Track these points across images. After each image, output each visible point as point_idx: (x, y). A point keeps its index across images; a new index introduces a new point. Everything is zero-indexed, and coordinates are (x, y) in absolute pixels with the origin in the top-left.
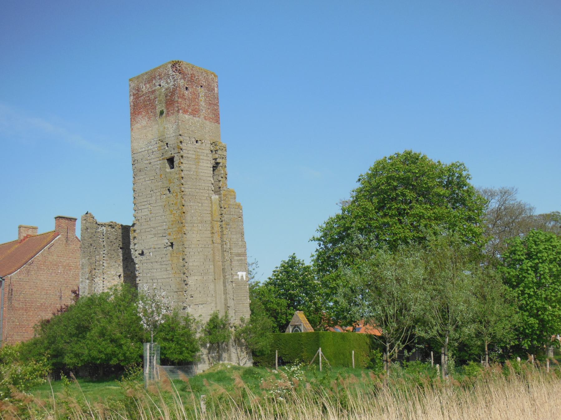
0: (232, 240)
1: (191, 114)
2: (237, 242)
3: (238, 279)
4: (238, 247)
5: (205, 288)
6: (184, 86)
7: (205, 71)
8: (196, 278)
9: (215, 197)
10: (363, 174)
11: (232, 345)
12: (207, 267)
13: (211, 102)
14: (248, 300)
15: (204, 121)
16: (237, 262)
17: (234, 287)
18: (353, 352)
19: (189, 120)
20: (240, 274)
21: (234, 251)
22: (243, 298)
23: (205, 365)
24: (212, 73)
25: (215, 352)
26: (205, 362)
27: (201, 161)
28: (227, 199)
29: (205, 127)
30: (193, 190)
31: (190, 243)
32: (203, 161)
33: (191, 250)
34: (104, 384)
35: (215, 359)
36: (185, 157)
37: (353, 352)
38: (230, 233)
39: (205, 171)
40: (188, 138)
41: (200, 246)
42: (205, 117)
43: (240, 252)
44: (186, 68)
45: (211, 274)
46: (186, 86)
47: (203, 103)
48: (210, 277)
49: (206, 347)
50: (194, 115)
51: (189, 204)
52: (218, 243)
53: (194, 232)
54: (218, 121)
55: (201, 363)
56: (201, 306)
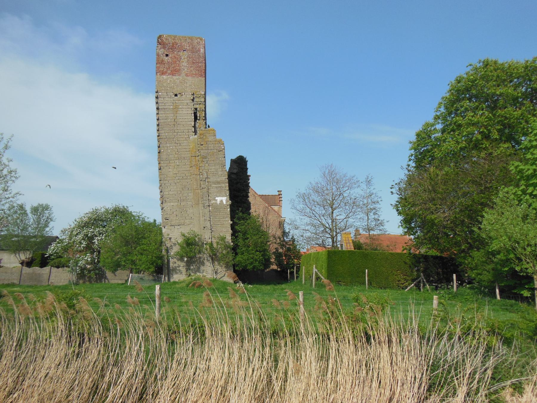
0: (210, 170)
1: (170, 74)
2: (216, 172)
3: (216, 203)
4: (217, 176)
5: (183, 213)
6: (164, 53)
7: (189, 38)
8: (172, 204)
9: (193, 137)
10: (441, 101)
11: (207, 260)
12: (186, 195)
13: (194, 61)
14: (229, 221)
15: (186, 77)
16: (216, 189)
17: (211, 210)
18: (367, 270)
19: (167, 79)
20: (219, 199)
21: (212, 180)
22: (221, 219)
23: (181, 275)
24: (198, 38)
25: (194, 265)
26: (181, 273)
27: (180, 110)
28: (204, 137)
29: (186, 82)
30: (171, 134)
31: (166, 176)
32: (183, 109)
33: (167, 182)
34: (259, 284)
35: (194, 271)
36: (161, 109)
37: (367, 270)
38: (207, 165)
39: (185, 117)
40: (165, 94)
41: (177, 178)
42: (187, 74)
43: (219, 180)
44: (166, 39)
45: (189, 200)
46: (166, 53)
47: (185, 64)
48: (188, 203)
49: (184, 260)
50: (173, 74)
51: (165, 146)
52: (196, 175)
53: (171, 167)
54: (204, 74)
55: (176, 273)
56: (176, 227)
